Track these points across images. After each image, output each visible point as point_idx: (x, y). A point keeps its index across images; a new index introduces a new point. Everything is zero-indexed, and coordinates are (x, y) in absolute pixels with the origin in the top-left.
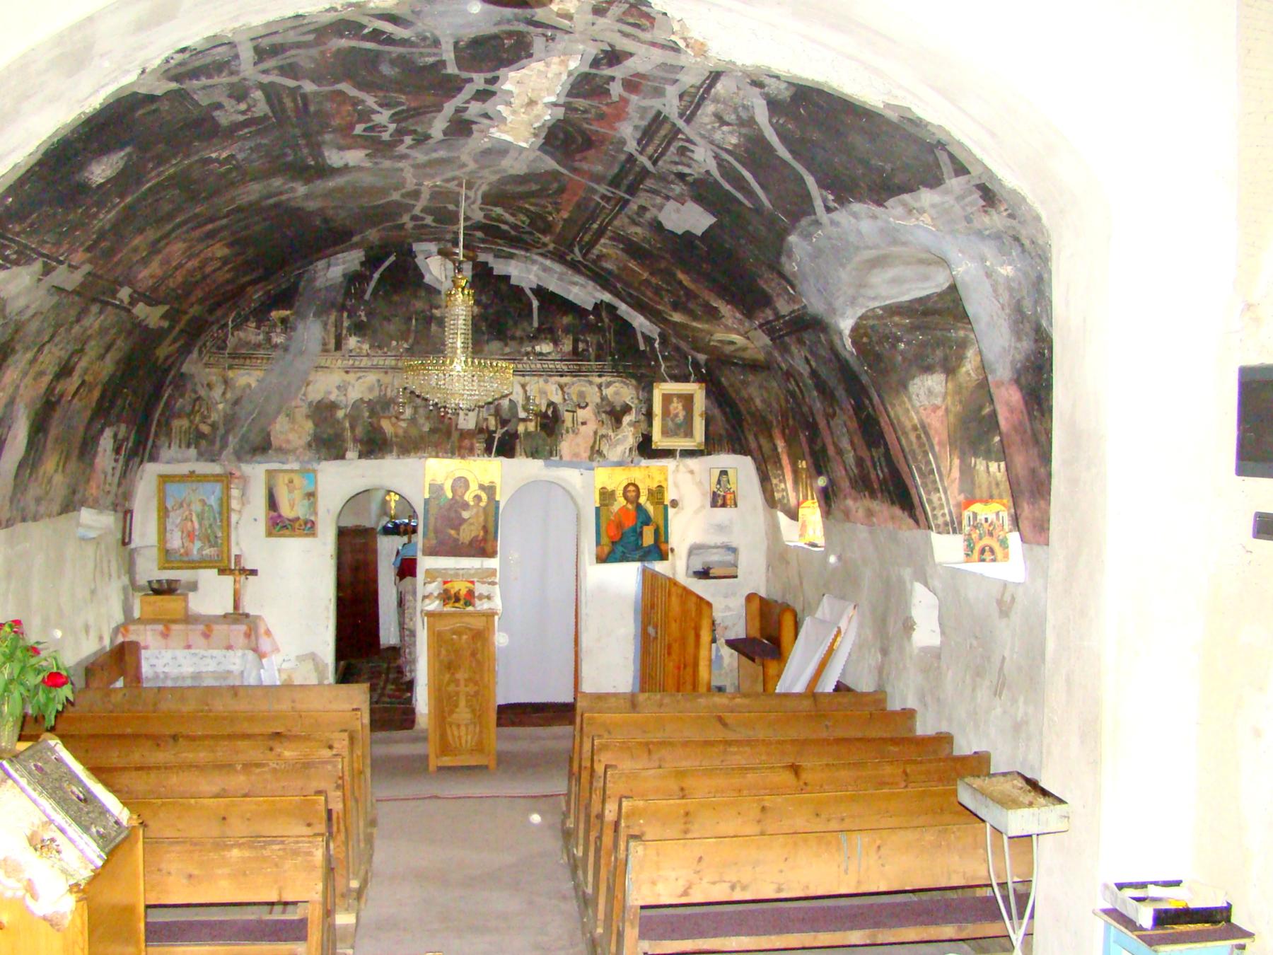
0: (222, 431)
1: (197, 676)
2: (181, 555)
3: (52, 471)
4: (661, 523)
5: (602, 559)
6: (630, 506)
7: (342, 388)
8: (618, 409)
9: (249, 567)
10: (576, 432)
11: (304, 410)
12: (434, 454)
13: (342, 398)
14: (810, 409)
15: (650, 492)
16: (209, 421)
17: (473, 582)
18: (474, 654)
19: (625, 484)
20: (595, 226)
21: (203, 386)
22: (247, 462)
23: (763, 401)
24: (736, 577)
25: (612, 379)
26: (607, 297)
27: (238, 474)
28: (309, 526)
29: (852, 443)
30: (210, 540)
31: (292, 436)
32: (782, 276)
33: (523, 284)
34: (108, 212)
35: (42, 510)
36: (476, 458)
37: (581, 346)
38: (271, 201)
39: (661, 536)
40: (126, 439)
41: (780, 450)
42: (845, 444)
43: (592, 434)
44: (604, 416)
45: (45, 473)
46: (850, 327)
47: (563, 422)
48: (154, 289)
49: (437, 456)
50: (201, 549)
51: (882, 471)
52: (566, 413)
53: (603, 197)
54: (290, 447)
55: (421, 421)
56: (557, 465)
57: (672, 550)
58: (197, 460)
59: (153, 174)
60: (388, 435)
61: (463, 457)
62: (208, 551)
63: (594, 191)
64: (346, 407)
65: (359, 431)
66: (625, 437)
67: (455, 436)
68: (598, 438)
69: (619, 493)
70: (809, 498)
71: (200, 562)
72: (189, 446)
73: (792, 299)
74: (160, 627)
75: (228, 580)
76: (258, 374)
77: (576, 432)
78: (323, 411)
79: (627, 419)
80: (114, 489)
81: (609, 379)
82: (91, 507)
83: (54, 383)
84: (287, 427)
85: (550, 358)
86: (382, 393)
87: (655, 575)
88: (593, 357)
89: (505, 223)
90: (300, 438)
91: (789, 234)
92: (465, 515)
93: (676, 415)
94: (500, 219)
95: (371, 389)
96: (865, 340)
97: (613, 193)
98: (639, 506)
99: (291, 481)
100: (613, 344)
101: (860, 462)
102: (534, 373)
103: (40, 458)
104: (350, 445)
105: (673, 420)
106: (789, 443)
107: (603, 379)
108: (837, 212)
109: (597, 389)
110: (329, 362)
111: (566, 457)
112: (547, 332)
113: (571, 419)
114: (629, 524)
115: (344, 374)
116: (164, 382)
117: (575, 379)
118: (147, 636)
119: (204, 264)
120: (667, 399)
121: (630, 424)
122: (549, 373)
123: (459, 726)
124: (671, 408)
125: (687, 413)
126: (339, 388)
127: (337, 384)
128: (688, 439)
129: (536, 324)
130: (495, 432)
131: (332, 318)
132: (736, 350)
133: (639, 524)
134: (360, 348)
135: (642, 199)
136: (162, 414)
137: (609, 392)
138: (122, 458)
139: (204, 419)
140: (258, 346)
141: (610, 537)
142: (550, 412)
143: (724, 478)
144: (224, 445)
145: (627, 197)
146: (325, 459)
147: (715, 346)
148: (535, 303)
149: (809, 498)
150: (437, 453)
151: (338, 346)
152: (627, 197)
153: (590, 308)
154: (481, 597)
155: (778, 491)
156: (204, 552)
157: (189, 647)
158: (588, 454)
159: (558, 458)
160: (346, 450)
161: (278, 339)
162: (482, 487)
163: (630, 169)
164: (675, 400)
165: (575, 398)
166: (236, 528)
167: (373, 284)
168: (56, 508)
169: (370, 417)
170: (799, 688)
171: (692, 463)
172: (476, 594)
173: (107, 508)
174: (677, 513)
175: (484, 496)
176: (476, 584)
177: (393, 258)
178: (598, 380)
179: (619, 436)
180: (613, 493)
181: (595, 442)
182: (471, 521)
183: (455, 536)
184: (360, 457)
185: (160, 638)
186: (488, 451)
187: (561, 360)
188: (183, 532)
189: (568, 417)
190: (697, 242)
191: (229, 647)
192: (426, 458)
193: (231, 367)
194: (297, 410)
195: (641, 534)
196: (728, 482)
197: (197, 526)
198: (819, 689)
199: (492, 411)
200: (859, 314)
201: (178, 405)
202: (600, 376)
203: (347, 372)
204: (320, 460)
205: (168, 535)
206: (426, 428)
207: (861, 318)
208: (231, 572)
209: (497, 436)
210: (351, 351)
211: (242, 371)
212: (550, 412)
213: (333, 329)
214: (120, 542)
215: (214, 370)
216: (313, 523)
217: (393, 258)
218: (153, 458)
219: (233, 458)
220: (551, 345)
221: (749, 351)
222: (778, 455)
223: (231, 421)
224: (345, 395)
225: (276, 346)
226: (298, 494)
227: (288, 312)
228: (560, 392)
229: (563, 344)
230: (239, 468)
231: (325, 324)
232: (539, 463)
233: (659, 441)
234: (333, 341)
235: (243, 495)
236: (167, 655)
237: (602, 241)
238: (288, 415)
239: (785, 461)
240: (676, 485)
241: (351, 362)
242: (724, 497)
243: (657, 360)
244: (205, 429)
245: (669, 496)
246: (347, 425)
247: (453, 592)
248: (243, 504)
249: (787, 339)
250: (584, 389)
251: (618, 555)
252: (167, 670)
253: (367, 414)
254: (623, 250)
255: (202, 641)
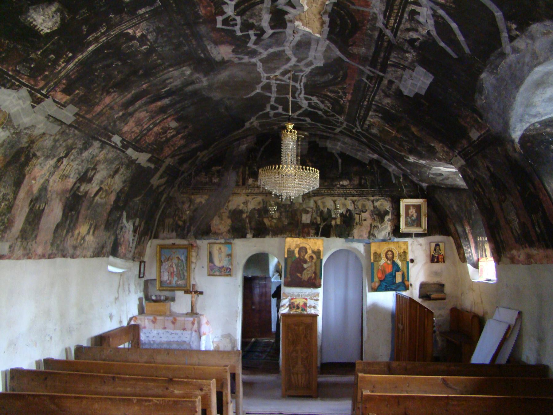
0: (188, 224)
1: (169, 343)
2: (168, 284)
3: (85, 233)
4: (405, 270)
5: (374, 290)
6: (389, 262)
7: (246, 203)
8: (382, 212)
9: (199, 290)
10: (361, 224)
11: (227, 214)
12: (290, 235)
13: (245, 208)
14: (489, 199)
15: (400, 255)
16: (183, 219)
17: (306, 299)
18: (306, 337)
19: (386, 250)
20: (366, 103)
21: (179, 202)
22: (200, 239)
23: (458, 206)
24: (444, 299)
25: (379, 198)
26: (375, 156)
27: (195, 245)
28: (228, 270)
29: (517, 214)
30: (180, 276)
31: (221, 227)
32: (475, 110)
33: (334, 151)
34: (68, 62)
35: (78, 252)
36: (311, 237)
37: (363, 181)
38: (190, 88)
39: (405, 277)
40: (140, 225)
41: (467, 232)
42: (513, 216)
43: (369, 225)
44: (375, 216)
45: (79, 234)
46: (519, 137)
47: (355, 219)
48: (137, 141)
49: (291, 237)
50: (177, 281)
51: (540, 228)
52: (356, 215)
53: (369, 78)
54: (219, 232)
55: (284, 219)
56: (352, 241)
57: (411, 285)
58: (176, 238)
59: (90, 38)
60: (267, 226)
61: (304, 237)
62: (181, 282)
63: (362, 72)
64: (247, 212)
65: (253, 223)
66: (386, 227)
67: (300, 227)
68: (372, 227)
69: (383, 255)
70: (484, 256)
71: (176, 287)
72: (172, 231)
73: (480, 127)
74: (151, 318)
75: (189, 296)
76: (206, 197)
77: (361, 224)
78: (236, 214)
79: (387, 218)
80: (133, 250)
81: (377, 198)
82: (122, 258)
83: (78, 185)
84: (218, 222)
85: (348, 187)
86: (265, 205)
87: (403, 297)
88: (369, 186)
89: (319, 109)
90: (224, 227)
91: (481, 73)
92: (305, 266)
93: (412, 216)
94: (316, 107)
95: (259, 203)
96: (529, 144)
97: (373, 73)
98: (394, 263)
99: (220, 249)
100: (379, 180)
101: (522, 225)
102: (339, 195)
103: (74, 225)
104: (249, 231)
105: (410, 218)
106: (472, 228)
107: (375, 197)
108: (518, 39)
109: (371, 203)
110: (239, 190)
111: (356, 237)
112: (345, 175)
113: (358, 218)
114: (389, 270)
115: (246, 196)
116: (160, 200)
117: (360, 198)
118: (145, 322)
119: (165, 131)
120: (407, 207)
121: (389, 220)
122: (346, 196)
123: (297, 374)
124: (410, 211)
125: (418, 214)
126: (244, 203)
127: (243, 202)
128: (418, 228)
129: (340, 171)
130: (320, 224)
131: (241, 170)
132: (443, 180)
133: (394, 272)
134: (254, 184)
135: (390, 74)
136: (161, 216)
137: (377, 204)
138: (137, 236)
139: (180, 218)
140: (206, 183)
141: (379, 278)
142: (347, 215)
143: (438, 248)
144: (189, 231)
145: (381, 74)
146: (237, 238)
147: (432, 178)
148: (340, 161)
149: (484, 256)
150: (291, 235)
151: (244, 184)
152: (381, 74)
153: (367, 162)
154: (310, 307)
155: (467, 253)
156: (178, 283)
157: (165, 328)
158: (367, 235)
159: (352, 238)
160: (247, 233)
161: (215, 180)
162: (313, 252)
163: (382, 44)
164: (411, 207)
165: (360, 207)
166: (194, 271)
167: (260, 153)
168: (89, 254)
169: (258, 217)
170: (487, 361)
171: (421, 240)
172: (308, 305)
173: (129, 259)
174: (413, 266)
175: (315, 256)
176: (308, 300)
177: (270, 140)
178: (372, 198)
179: (383, 227)
180: (380, 255)
181: (371, 230)
182: (308, 269)
183: (301, 277)
184: (253, 237)
185: (151, 323)
186: (317, 234)
187: (353, 189)
188: (168, 272)
189: (357, 217)
190: (422, 101)
191: (184, 329)
192: (286, 238)
193: (193, 194)
194: (223, 214)
195: (395, 276)
196: (440, 249)
197: (175, 270)
198: (498, 362)
199: (319, 214)
200: (525, 128)
201: (168, 212)
202: (373, 196)
203: (248, 196)
204: (234, 238)
205: (162, 274)
206: (286, 223)
207: (525, 130)
208: (191, 292)
209: (321, 226)
210: (250, 185)
211: (198, 196)
212: (347, 215)
213: (242, 175)
214: (138, 276)
215: (185, 195)
216: (230, 269)
217: (270, 140)
218: (156, 237)
219: (193, 237)
220: (348, 181)
221: (450, 180)
222: (466, 234)
223: (192, 219)
224: (247, 207)
225: (215, 183)
226: (223, 255)
227: (220, 168)
228: (353, 204)
229: (354, 181)
230: (196, 243)
231: (237, 173)
232: (342, 240)
233: (403, 228)
234: (241, 181)
235: (197, 255)
236: (155, 332)
237: (371, 113)
238: (219, 217)
239: (470, 237)
240: (413, 252)
241: (250, 191)
242: (438, 258)
243: (401, 188)
244: (180, 223)
245: (410, 257)
246: (247, 221)
247: (296, 304)
248: (197, 260)
249: (475, 157)
250: (364, 203)
251: (383, 287)
252: (154, 339)
253: (257, 216)
254: (381, 118)
255: (171, 325)
